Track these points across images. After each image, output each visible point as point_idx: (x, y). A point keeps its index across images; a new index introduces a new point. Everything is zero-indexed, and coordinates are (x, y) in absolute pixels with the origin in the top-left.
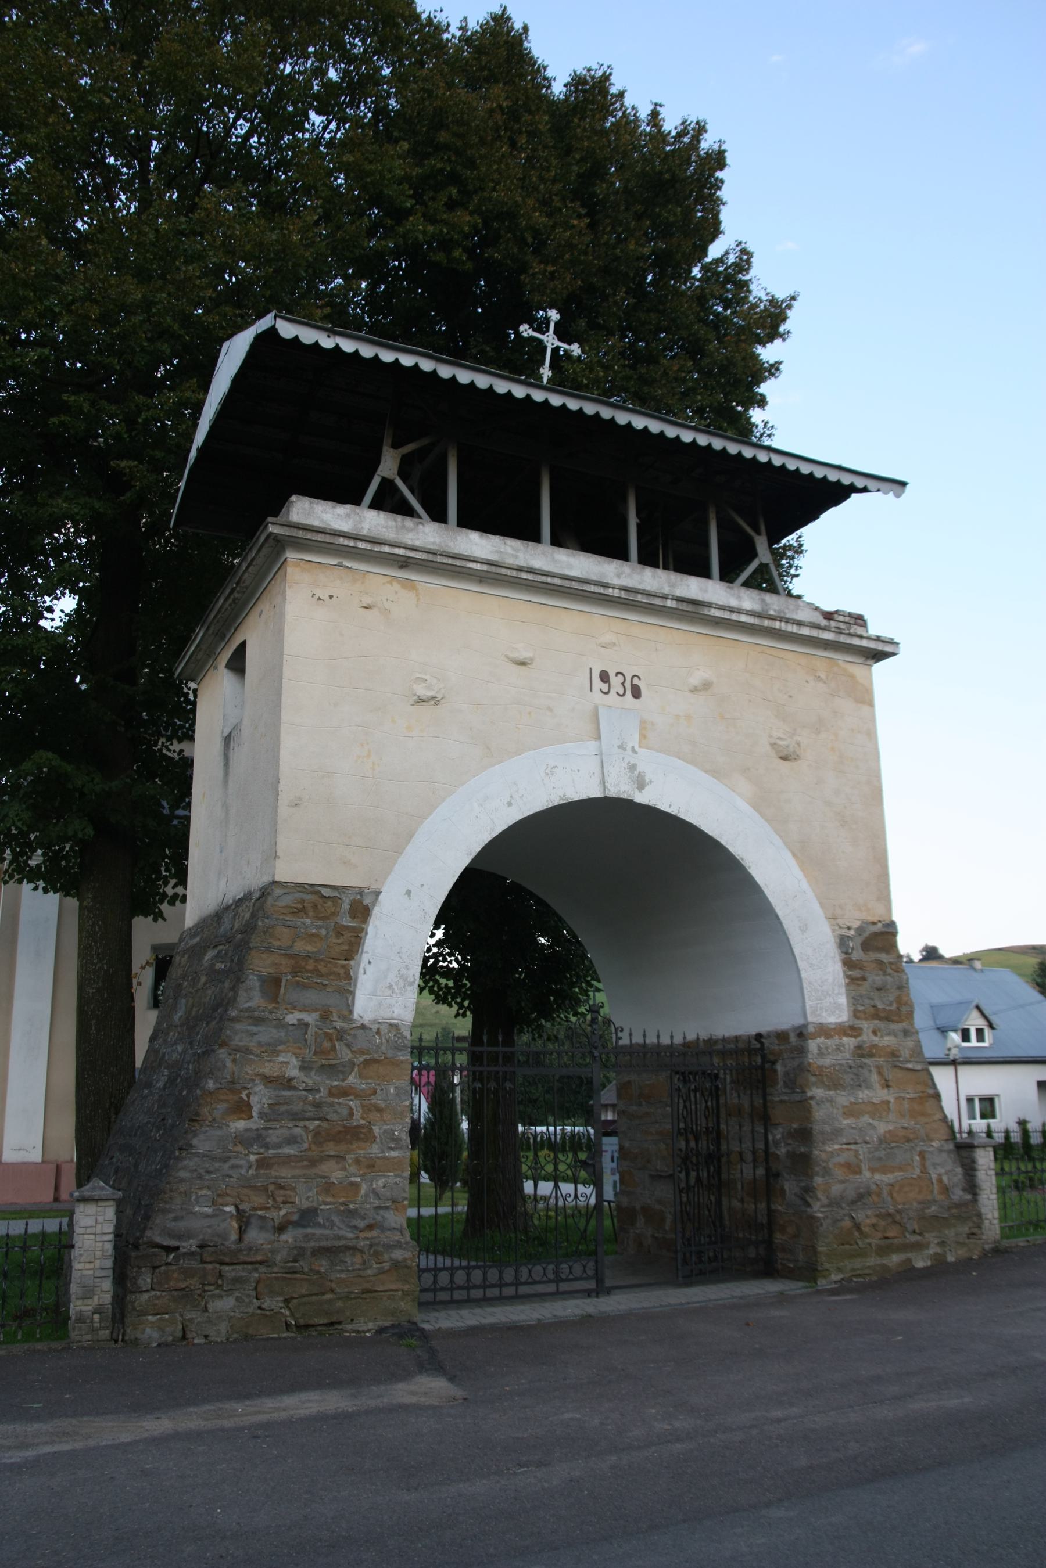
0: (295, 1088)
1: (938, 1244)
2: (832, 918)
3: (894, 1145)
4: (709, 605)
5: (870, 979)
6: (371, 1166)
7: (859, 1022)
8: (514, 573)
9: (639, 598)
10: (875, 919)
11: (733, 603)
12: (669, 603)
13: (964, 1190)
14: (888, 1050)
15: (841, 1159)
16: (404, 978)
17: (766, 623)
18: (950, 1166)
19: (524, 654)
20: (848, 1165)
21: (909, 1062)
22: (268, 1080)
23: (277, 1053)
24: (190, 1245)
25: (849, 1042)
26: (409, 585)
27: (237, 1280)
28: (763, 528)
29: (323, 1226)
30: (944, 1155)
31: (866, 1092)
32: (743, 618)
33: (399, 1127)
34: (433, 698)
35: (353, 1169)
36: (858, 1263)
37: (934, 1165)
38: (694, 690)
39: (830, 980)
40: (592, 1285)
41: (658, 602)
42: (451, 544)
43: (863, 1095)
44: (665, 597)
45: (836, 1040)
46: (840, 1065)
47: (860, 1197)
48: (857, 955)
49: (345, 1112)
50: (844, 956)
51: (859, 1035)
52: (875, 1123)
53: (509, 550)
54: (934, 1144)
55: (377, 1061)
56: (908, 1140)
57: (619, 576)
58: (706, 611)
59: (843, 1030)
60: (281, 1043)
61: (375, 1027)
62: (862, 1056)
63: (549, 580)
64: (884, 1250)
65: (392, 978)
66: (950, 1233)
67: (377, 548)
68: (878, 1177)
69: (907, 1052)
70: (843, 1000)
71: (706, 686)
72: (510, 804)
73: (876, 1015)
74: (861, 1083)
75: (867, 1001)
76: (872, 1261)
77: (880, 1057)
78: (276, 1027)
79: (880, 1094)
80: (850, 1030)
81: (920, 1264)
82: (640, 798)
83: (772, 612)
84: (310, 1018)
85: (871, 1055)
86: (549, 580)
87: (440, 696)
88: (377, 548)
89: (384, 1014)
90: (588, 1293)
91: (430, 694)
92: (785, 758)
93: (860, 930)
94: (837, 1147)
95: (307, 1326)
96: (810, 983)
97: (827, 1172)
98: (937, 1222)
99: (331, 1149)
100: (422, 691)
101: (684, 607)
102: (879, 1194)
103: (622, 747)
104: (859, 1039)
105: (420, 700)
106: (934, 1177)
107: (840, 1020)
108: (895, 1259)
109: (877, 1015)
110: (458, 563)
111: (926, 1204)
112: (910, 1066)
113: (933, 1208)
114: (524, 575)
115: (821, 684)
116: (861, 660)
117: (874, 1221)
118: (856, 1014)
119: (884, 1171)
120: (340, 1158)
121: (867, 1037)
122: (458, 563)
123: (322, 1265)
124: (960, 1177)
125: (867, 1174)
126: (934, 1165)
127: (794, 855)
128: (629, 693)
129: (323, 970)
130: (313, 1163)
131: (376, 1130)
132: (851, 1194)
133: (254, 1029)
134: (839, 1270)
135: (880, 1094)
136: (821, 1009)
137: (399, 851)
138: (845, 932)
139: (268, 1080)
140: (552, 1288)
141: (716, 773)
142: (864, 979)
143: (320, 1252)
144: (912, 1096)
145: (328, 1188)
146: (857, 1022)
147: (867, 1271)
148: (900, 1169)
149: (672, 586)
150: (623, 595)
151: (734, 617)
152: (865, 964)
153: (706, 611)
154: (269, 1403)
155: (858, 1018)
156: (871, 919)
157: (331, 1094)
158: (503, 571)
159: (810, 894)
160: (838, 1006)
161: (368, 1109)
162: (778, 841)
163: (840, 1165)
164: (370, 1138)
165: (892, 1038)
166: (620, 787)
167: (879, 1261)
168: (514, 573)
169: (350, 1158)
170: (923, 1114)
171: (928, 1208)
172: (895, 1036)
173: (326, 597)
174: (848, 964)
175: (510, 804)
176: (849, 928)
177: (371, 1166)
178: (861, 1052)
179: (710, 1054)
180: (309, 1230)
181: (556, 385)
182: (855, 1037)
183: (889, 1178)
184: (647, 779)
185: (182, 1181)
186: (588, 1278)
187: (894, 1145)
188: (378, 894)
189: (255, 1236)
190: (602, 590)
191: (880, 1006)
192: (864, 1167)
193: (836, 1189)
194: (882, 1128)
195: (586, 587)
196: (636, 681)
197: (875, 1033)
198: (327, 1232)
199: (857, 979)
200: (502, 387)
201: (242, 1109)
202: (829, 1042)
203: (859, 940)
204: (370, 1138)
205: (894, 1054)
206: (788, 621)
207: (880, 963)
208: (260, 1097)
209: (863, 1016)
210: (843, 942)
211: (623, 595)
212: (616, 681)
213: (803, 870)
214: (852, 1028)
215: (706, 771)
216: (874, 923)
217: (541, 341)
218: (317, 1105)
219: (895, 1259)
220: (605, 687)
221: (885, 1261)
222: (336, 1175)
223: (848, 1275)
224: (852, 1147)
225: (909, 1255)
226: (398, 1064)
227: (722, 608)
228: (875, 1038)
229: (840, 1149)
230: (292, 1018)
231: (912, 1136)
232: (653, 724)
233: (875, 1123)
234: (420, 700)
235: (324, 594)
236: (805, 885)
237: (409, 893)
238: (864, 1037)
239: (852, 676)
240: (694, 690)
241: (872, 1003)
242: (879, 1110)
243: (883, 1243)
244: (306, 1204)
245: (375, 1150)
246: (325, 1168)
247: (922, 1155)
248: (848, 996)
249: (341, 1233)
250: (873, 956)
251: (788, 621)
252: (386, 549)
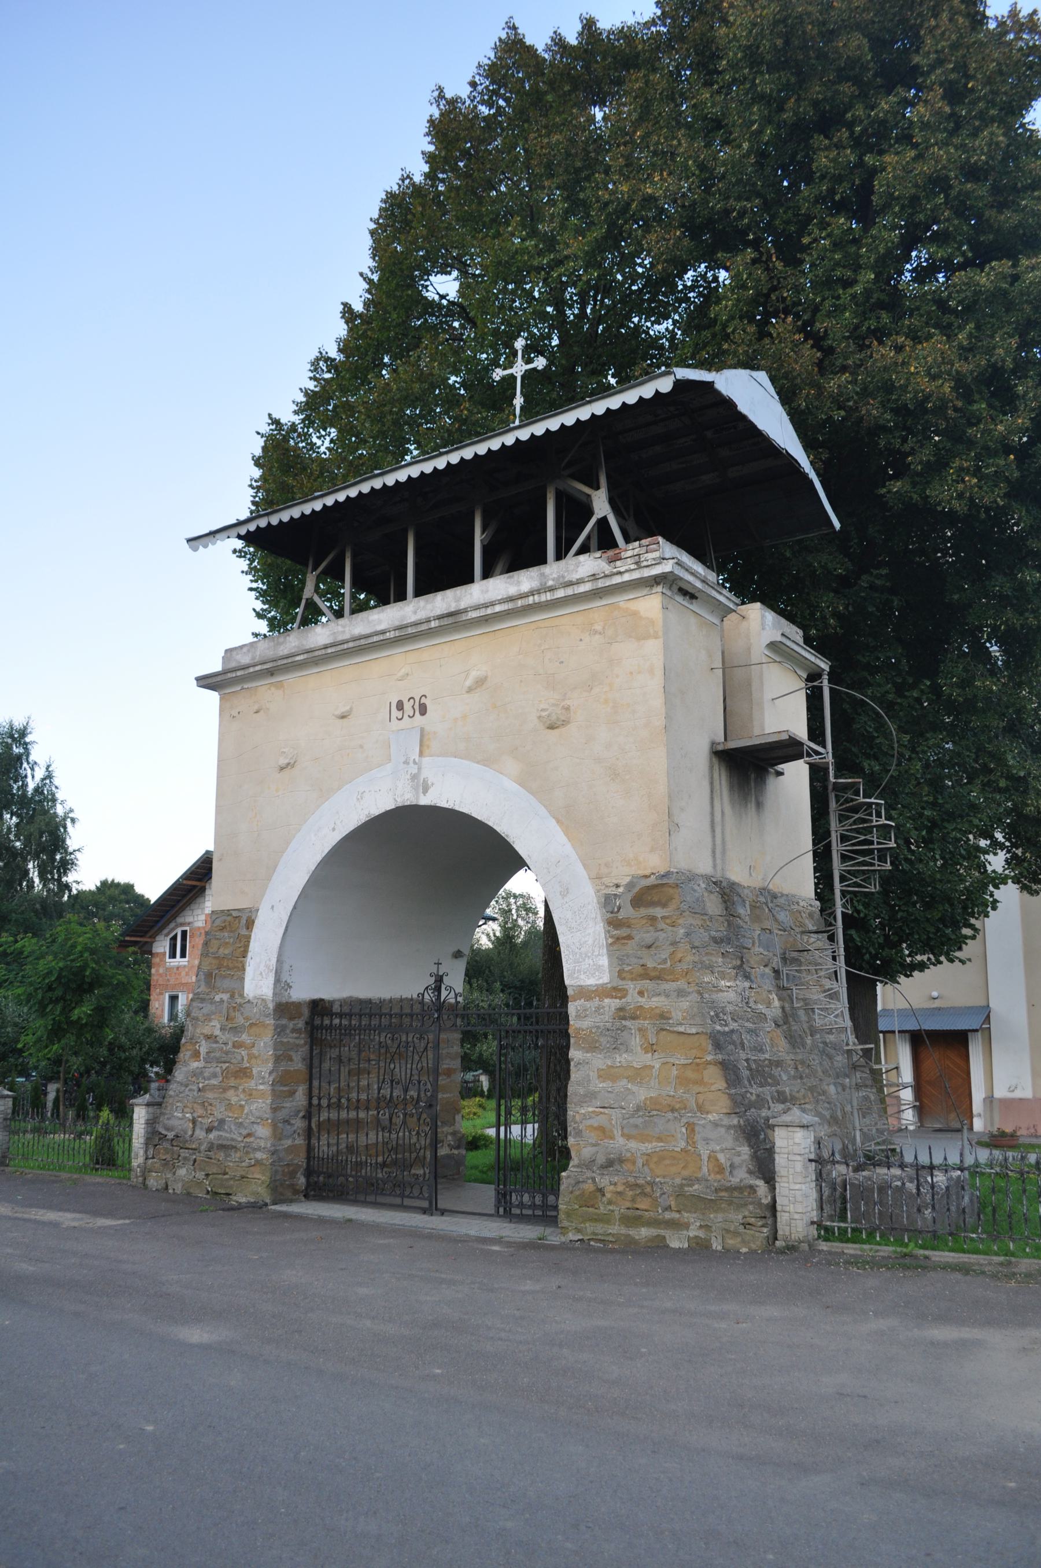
0: (217, 1042)
1: (701, 1226)
2: (597, 878)
3: (655, 1113)
4: (465, 611)
5: (637, 938)
6: (250, 1094)
7: (624, 982)
8: (323, 652)
9: (410, 630)
10: (647, 872)
11: (513, 591)
12: (433, 624)
13: (750, 1172)
14: (658, 1011)
15: (595, 1122)
16: (267, 966)
17: (520, 603)
18: (729, 1143)
19: (343, 709)
20: (601, 1129)
21: (681, 1024)
22: (208, 1037)
23: (210, 1020)
24: (170, 1135)
25: (611, 1004)
26: (279, 685)
27: (185, 1158)
28: (603, 481)
29: (227, 1131)
30: (723, 1130)
31: (625, 1055)
32: (498, 608)
33: (264, 1069)
34: (288, 764)
35: (242, 1096)
36: (599, 1228)
37: (707, 1140)
38: (470, 690)
39: (590, 942)
40: (425, 1204)
41: (424, 627)
42: (304, 643)
43: (621, 1058)
44: (428, 621)
45: (596, 1002)
46: (598, 1027)
47: (610, 1164)
48: (627, 912)
49: (240, 1058)
50: (609, 915)
51: (624, 996)
52: (635, 1088)
53: (340, 629)
54: (710, 1116)
55: (255, 1024)
56: (673, 1110)
57: (415, 613)
58: (464, 617)
59: (602, 992)
60: (214, 1014)
61: (255, 1001)
62: (624, 1018)
63: (345, 646)
64: (633, 1220)
65: (262, 968)
66: (717, 1218)
67: (247, 672)
68: (633, 1145)
69: (680, 1014)
70: (604, 961)
71: (481, 682)
72: (334, 829)
73: (645, 974)
74: (617, 1046)
75: (634, 960)
76: (616, 1229)
77: (645, 1019)
78: (211, 1003)
79: (639, 1058)
80: (614, 991)
81: (675, 1244)
82: (424, 801)
83: (550, 583)
84: (225, 997)
85: (634, 1018)
86: (345, 646)
87: (292, 762)
88: (247, 672)
89: (259, 992)
90: (425, 1211)
91: (287, 761)
92: (551, 727)
93: (630, 886)
94: (590, 1109)
95: (216, 1193)
96: (568, 946)
97: (579, 1133)
98: (701, 1204)
99: (232, 1082)
100: (283, 761)
101: (446, 621)
102: (634, 1163)
103: (406, 762)
104: (623, 1000)
105: (282, 769)
106: (705, 1154)
107: (601, 982)
108: (644, 1233)
109: (647, 974)
110: (290, 660)
111: (691, 1181)
112: (681, 1029)
113: (696, 1187)
114: (329, 651)
115: (597, 636)
116: (646, 591)
117: (620, 1188)
118: (621, 975)
119: (643, 1139)
120: (236, 1088)
121: (632, 999)
122: (290, 660)
123: (221, 1156)
124: (746, 1157)
125: (621, 1140)
126: (707, 1140)
127: (558, 821)
128: (417, 712)
129: (231, 965)
130: (225, 1090)
131: (255, 1071)
132: (601, 1159)
133: (201, 1005)
134: (579, 1231)
135: (639, 1058)
136: (579, 971)
137: (269, 878)
138: (612, 891)
139: (208, 1037)
140: (398, 1201)
141: (487, 762)
142: (629, 937)
143: (222, 1147)
144: (683, 1062)
145: (229, 1106)
146: (621, 983)
147: (611, 1239)
148: (660, 1139)
149: (458, 600)
150: (510, 606)
151: (489, 611)
152: (633, 921)
153: (464, 617)
154: (42, 1212)
155: (623, 979)
156: (641, 872)
157: (234, 1046)
158: (317, 653)
159: (574, 856)
160: (599, 968)
161: (251, 1057)
162: (543, 811)
163: (592, 1128)
164: (250, 1076)
165: (662, 998)
166: (406, 796)
167: (623, 1231)
168: (323, 652)
169: (241, 1088)
170: (700, 1082)
171: (691, 1186)
172: (667, 996)
173: (236, 714)
174: (614, 922)
175: (334, 829)
176: (617, 886)
177: (250, 1094)
178: (622, 1013)
179: (361, 1016)
180: (221, 1133)
181: (531, 414)
182: (620, 998)
183: (648, 1147)
184: (429, 783)
185: (171, 1096)
186: (424, 1199)
187: (655, 1113)
188: (258, 910)
189: (200, 1134)
190: (381, 637)
191: (650, 964)
192: (617, 1133)
193: (587, 1152)
194: (642, 1094)
195: (370, 640)
196: (423, 700)
197: (641, 993)
198: (228, 1135)
199: (624, 938)
200: (481, 449)
201: (196, 1055)
202: (588, 1004)
203: (629, 896)
204: (250, 1076)
205: (664, 1016)
206: (570, 584)
207: (653, 919)
208: (203, 1048)
209: (629, 976)
210: (608, 901)
211: (510, 606)
212: (407, 706)
213: (567, 835)
214: (615, 989)
215: (478, 763)
216: (646, 877)
217: (523, 377)
218: (227, 1053)
219: (644, 1233)
220: (399, 714)
221: (632, 1232)
222: (234, 1100)
223: (586, 1238)
224: (606, 1111)
225: (662, 1232)
226: (265, 1026)
227: (477, 608)
228: (640, 999)
229: (593, 1112)
230: (217, 998)
231: (677, 1106)
232: (435, 733)
233: (635, 1088)
234: (282, 769)
235: (234, 713)
236: (568, 849)
237: (273, 907)
238: (629, 999)
239: (635, 614)
240: (470, 690)
241: (642, 962)
242: (638, 1075)
243: (630, 1213)
244: (220, 1117)
245: (252, 1084)
246: (231, 1093)
247: (691, 1127)
248: (610, 956)
249: (235, 1137)
250: (643, 911)
251: (570, 584)
252: (251, 670)
